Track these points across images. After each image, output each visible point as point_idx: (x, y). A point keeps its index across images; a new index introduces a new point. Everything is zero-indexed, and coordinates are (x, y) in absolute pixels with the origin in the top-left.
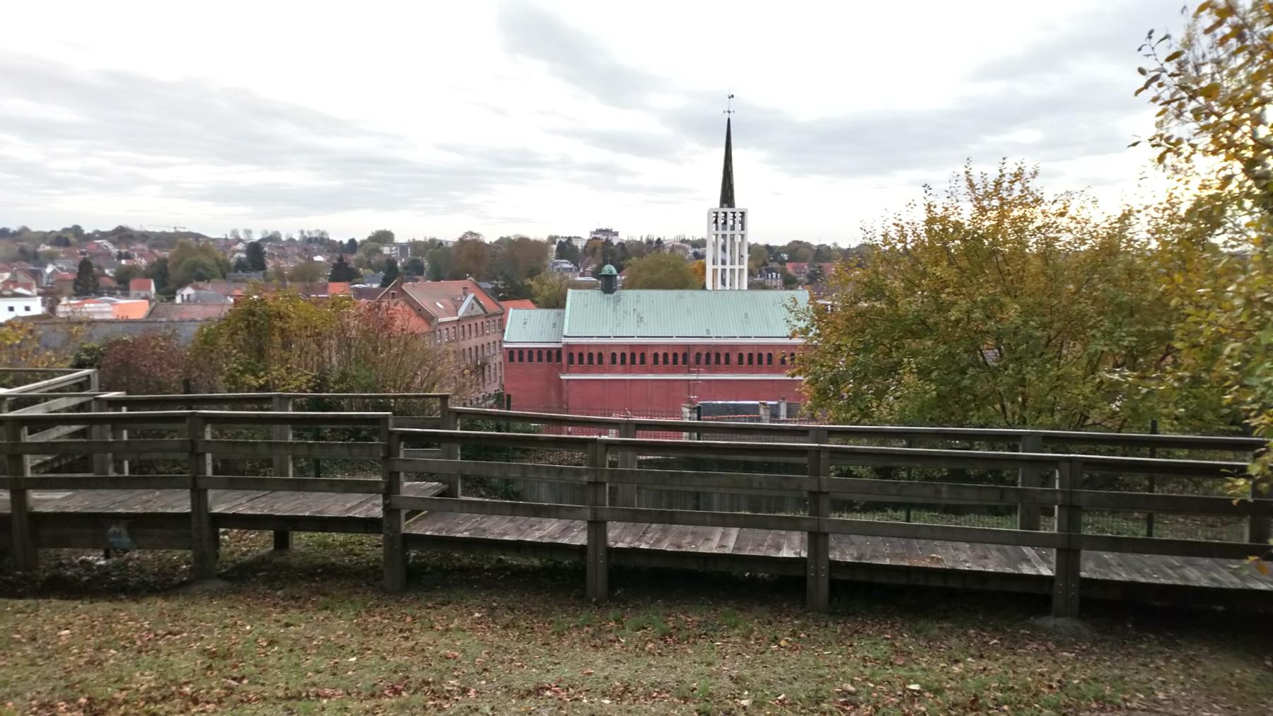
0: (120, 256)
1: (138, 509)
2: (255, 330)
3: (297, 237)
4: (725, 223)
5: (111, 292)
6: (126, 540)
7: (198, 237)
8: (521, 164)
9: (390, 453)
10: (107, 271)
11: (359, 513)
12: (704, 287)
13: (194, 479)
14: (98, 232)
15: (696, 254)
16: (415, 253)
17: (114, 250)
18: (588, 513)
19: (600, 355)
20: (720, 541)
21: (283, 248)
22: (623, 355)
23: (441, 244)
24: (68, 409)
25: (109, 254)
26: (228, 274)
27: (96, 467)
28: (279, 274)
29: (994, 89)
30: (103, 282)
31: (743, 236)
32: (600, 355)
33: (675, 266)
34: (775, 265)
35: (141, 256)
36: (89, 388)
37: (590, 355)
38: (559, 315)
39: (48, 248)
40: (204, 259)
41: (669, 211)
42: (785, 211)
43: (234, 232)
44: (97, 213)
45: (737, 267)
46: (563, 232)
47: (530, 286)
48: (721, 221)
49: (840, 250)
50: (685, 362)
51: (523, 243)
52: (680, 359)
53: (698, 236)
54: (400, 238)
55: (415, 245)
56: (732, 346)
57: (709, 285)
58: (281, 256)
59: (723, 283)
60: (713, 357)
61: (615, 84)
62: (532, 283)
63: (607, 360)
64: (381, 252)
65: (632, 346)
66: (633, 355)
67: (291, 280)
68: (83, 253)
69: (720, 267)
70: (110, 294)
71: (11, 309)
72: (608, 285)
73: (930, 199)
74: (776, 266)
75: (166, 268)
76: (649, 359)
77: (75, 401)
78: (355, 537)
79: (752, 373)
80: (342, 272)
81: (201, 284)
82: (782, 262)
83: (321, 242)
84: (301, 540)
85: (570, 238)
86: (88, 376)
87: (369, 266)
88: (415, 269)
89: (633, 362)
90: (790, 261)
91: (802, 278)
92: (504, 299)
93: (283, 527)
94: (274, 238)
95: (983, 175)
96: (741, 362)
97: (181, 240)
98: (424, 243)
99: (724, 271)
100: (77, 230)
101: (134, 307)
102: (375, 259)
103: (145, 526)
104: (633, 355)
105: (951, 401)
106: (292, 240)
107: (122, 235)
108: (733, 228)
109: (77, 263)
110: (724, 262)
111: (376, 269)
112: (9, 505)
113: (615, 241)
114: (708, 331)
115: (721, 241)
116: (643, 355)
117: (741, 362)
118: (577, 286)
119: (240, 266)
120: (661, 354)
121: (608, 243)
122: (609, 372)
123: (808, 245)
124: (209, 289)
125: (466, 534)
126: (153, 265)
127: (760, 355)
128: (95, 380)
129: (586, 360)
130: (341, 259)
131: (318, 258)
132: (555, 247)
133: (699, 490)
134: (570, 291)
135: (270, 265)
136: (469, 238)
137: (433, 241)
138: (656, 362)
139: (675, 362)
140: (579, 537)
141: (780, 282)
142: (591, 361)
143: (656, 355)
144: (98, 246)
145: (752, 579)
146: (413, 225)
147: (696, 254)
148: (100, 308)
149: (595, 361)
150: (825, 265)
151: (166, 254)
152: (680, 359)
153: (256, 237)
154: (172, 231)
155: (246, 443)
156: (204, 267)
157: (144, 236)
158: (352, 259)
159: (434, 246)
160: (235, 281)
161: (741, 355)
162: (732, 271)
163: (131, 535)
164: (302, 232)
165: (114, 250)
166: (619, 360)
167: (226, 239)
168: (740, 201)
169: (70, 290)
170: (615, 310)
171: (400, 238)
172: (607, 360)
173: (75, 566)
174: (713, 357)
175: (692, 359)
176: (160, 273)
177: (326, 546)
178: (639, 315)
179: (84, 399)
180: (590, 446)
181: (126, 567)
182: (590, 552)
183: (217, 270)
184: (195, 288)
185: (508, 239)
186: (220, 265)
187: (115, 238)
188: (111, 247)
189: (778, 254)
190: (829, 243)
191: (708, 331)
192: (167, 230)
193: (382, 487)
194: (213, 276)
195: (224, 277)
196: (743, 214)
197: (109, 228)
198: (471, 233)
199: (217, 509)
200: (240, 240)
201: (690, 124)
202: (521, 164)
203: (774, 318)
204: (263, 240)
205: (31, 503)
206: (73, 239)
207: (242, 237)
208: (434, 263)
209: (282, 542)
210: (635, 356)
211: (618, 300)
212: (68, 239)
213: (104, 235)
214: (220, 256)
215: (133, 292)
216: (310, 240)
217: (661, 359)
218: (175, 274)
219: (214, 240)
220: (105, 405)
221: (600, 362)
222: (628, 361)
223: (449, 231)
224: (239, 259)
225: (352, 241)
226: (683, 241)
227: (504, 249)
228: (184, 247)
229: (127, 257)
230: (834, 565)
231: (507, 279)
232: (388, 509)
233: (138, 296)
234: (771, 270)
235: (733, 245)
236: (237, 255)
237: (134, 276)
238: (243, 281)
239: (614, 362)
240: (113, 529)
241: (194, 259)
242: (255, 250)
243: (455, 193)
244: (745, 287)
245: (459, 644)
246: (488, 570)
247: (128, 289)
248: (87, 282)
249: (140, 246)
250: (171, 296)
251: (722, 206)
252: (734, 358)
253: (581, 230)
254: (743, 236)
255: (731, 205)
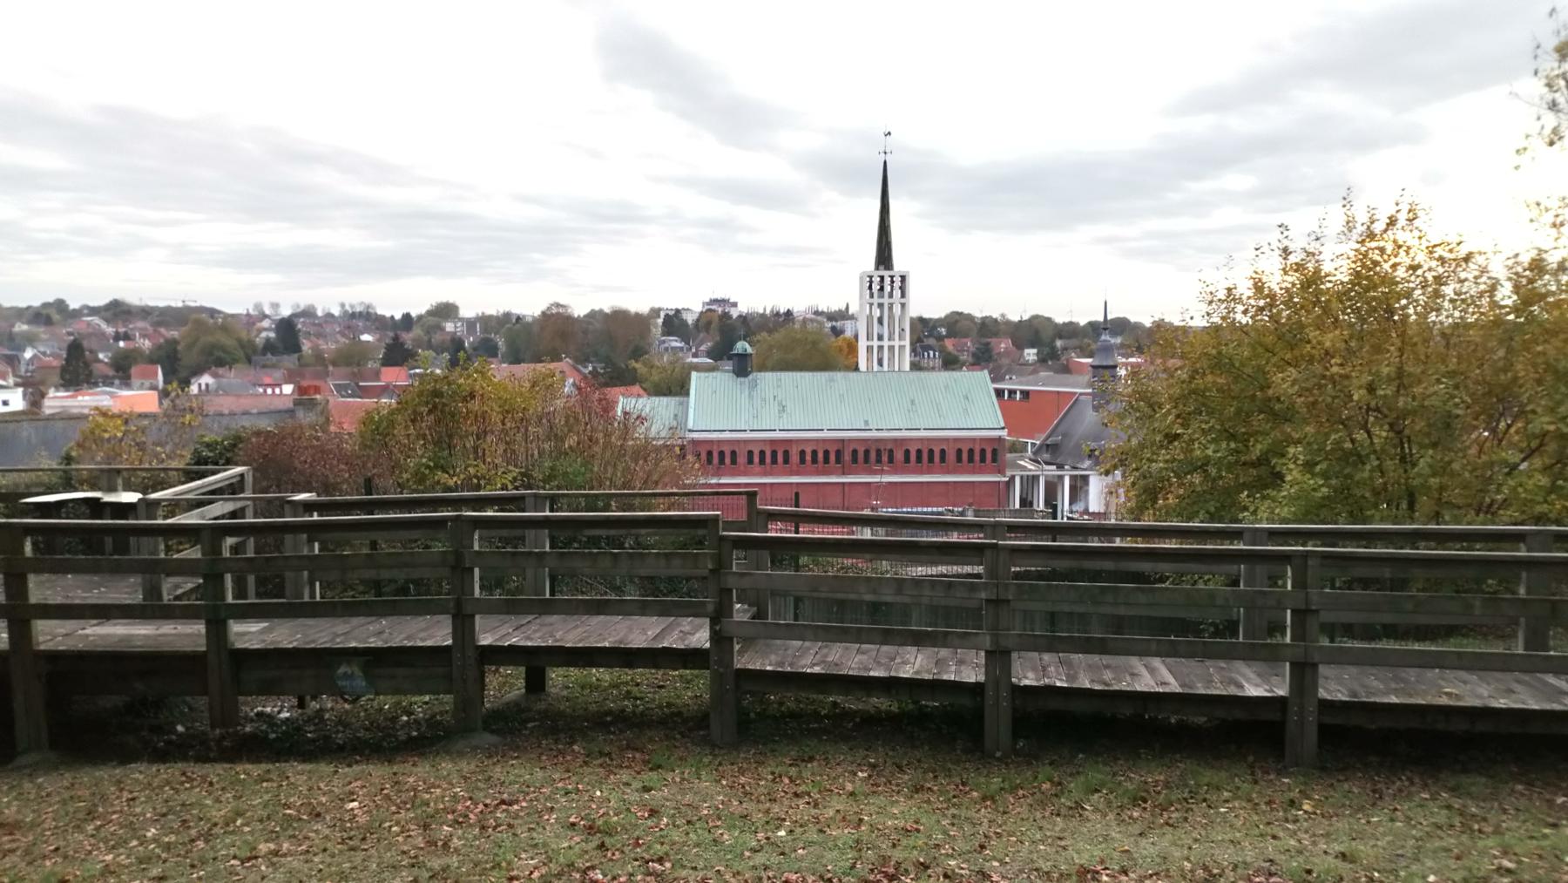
0: (117, 337)
1: (374, 643)
2: (439, 412)
3: (336, 312)
4: (882, 289)
5: (108, 381)
6: (361, 683)
7: (213, 312)
8: (618, 219)
9: (721, 565)
10: (101, 356)
11: (672, 641)
12: (856, 369)
13: (459, 603)
14: (88, 307)
15: (833, 329)
16: (485, 330)
17: (110, 330)
18: (987, 641)
19: (733, 453)
20: (1152, 676)
21: (320, 325)
22: (762, 453)
23: (519, 318)
24: (223, 517)
25: (103, 334)
26: (254, 358)
27: (289, 590)
28: (319, 357)
29: (1200, 125)
30: (98, 369)
31: (903, 305)
32: (733, 453)
33: (814, 343)
34: (932, 341)
35: (144, 336)
36: (242, 491)
37: (722, 454)
38: (681, 404)
39: (25, 327)
40: (229, 342)
41: (813, 274)
42: (954, 275)
43: (258, 306)
44: (86, 283)
45: (896, 343)
46: (669, 303)
47: (635, 369)
48: (876, 287)
49: (1008, 323)
50: (838, 461)
51: (619, 316)
52: (832, 457)
53: (835, 305)
54: (467, 312)
55: (485, 320)
56: (896, 441)
57: (863, 365)
58: (319, 335)
59: (880, 363)
60: (873, 455)
61: (737, 120)
62: (637, 366)
63: (742, 459)
64: (443, 329)
65: (773, 442)
66: (774, 453)
67: (334, 364)
68: (69, 334)
69: (875, 343)
70: (105, 385)
71: (5, 403)
72: (743, 367)
73: (1286, 243)
74: (952, 342)
75: (175, 351)
76: (795, 458)
77: (230, 507)
78: (626, 675)
79: (921, 473)
80: (397, 354)
81: (221, 371)
82: (940, 338)
83: (368, 318)
84: (558, 678)
85: (678, 311)
86: (242, 475)
87: (429, 346)
88: (487, 349)
89: (774, 461)
90: (949, 336)
91: (964, 357)
92: (606, 385)
93: (536, 662)
94: (308, 313)
95: (1371, 210)
96: (907, 460)
97: (194, 316)
98: (497, 318)
99: (881, 348)
100: (60, 305)
101: (140, 398)
102: (437, 338)
103: (383, 663)
104: (774, 453)
105: (1346, 499)
106: (329, 315)
107: (117, 311)
108: (891, 295)
109: (65, 345)
110: (880, 338)
111: (439, 350)
112: (203, 641)
113: (734, 313)
114: (866, 422)
115: (877, 313)
116: (786, 453)
117: (907, 460)
118: (697, 368)
119: (269, 347)
120: (808, 451)
121: (726, 315)
122: (745, 474)
123: (970, 317)
124: (232, 377)
125: (817, 670)
126: (160, 347)
127: (931, 452)
128: (249, 479)
129: (716, 460)
130: (396, 338)
131: (366, 337)
132: (660, 321)
133: (1057, 608)
134: (694, 375)
135: (306, 346)
136: (554, 311)
137: (507, 315)
138: (803, 461)
139: (826, 460)
140: (972, 673)
141: (938, 362)
142: (722, 461)
143: (803, 453)
144: (89, 324)
145: (1182, 726)
146: (482, 295)
147: (833, 329)
148: (86, 401)
149: (728, 460)
150: (993, 341)
151: (174, 334)
152: (832, 457)
153: (286, 312)
154: (180, 305)
155: (530, 553)
156: (223, 348)
157: (145, 312)
158: (408, 338)
159: (507, 322)
160: (264, 366)
161: (907, 452)
162: (891, 348)
163: (368, 676)
164: (343, 305)
165: (110, 330)
166: (756, 459)
167: (248, 315)
168: (900, 263)
169: (56, 379)
170: (750, 396)
171: (467, 312)
172: (742, 459)
173: (252, 720)
174: (873, 455)
175: (847, 457)
176: (168, 357)
177: (594, 688)
178: (780, 404)
179: (239, 505)
180: (988, 553)
181: (322, 719)
182: (990, 693)
183: (240, 354)
184: (215, 376)
185: (601, 311)
186: (242, 346)
187: (108, 314)
188: (104, 326)
189: (934, 327)
190: (995, 315)
191: (866, 422)
192: (173, 304)
193: (710, 608)
194: (235, 361)
195: (249, 361)
196: (903, 278)
197: (101, 301)
198: (558, 305)
199: (485, 640)
200: (266, 316)
201: (832, 170)
202: (618, 219)
203: (966, 406)
204: (294, 315)
205: (232, 638)
206: (56, 317)
207: (267, 312)
208: (511, 344)
209: (536, 682)
210: (777, 454)
211: (753, 386)
212: (50, 315)
213: (94, 311)
214: (244, 335)
215: (135, 382)
216: (353, 315)
217: (808, 458)
218: (188, 359)
219: (233, 316)
220: (301, 509)
221: (734, 461)
222: (768, 460)
223: (529, 303)
224: (268, 339)
225: (407, 317)
226: (817, 313)
227: (598, 326)
228: (199, 323)
229: (126, 337)
230: (1326, 705)
231: (608, 361)
232: (716, 637)
233: (141, 387)
234: (928, 348)
235: (891, 317)
236: (264, 334)
237: (136, 361)
238: (274, 366)
239: (750, 461)
240: (342, 670)
241: (210, 339)
242: (287, 328)
243: (536, 256)
244: (907, 368)
245: (547, 811)
246: (826, 716)
247: (129, 377)
248: (77, 369)
249: (140, 324)
250: (186, 383)
251: (877, 268)
252: (899, 455)
253: (693, 303)
254: (903, 305)
255: (889, 266)
